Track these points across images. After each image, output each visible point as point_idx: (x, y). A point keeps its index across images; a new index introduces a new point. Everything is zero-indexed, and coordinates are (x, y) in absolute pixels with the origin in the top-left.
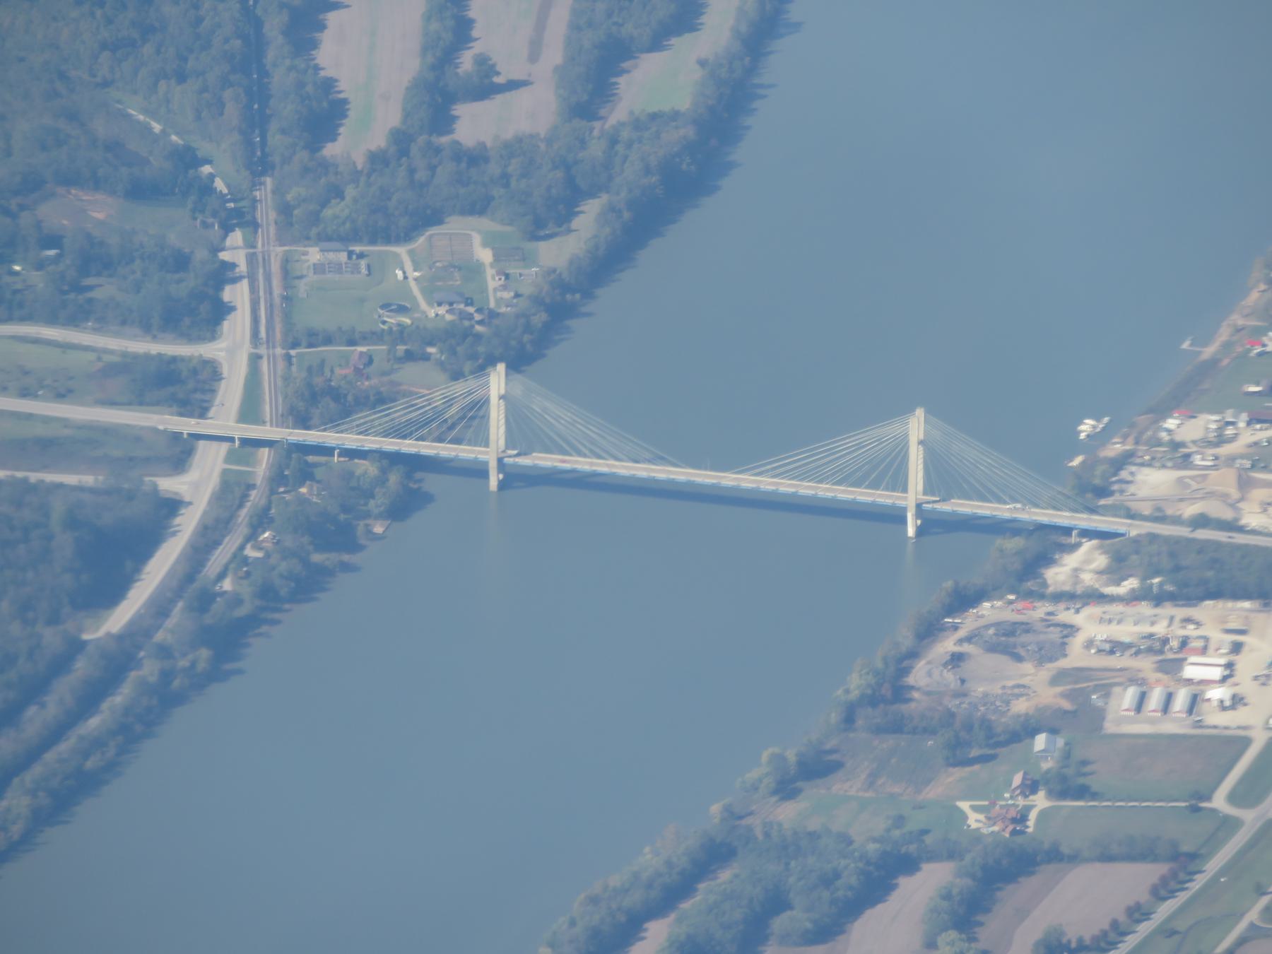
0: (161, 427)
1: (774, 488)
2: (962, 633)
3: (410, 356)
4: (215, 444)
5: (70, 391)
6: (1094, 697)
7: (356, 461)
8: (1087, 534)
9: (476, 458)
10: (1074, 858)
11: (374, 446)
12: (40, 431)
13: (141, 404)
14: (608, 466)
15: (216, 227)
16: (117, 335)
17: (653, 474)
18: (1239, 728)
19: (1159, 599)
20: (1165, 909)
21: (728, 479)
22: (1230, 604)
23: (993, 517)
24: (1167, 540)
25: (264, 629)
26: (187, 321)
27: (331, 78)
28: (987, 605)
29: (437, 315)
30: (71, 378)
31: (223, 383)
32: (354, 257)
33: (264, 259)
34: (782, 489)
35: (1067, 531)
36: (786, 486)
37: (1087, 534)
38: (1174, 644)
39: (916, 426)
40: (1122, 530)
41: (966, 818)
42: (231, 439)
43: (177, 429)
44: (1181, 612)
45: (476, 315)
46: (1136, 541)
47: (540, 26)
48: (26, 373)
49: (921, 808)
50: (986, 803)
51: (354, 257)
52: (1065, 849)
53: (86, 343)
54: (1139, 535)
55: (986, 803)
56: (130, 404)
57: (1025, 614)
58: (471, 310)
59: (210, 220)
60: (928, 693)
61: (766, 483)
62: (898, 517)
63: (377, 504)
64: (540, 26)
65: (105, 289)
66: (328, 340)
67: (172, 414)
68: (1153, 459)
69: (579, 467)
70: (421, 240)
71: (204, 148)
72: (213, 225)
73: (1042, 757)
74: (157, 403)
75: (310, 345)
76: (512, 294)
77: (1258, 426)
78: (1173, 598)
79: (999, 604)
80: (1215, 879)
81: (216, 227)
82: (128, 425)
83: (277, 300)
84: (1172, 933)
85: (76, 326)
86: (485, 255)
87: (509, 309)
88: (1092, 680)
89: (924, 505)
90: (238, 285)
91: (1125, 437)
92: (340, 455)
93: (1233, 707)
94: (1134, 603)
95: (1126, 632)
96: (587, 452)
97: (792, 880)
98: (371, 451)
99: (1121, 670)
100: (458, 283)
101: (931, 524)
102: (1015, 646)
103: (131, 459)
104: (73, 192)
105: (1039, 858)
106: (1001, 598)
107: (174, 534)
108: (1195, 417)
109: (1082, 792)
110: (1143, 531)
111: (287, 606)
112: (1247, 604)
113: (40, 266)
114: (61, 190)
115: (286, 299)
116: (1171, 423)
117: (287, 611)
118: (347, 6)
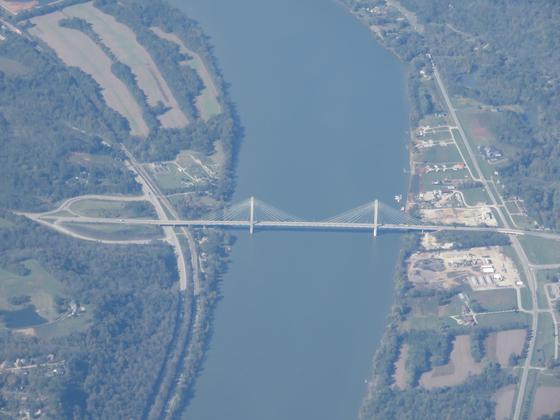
0: (152, 224)
1: (335, 226)
2: (413, 264)
3: (201, 195)
4: (168, 227)
5: (120, 215)
6: (464, 280)
7: (209, 228)
8: (426, 231)
9: (364, 227)
10: (497, 330)
11: (215, 224)
12: (121, 228)
13: (141, 217)
14: (285, 223)
15: (121, 160)
16: (115, 196)
17: (299, 225)
18: (509, 286)
19: (458, 248)
20: (532, 343)
21: (321, 224)
22: (478, 249)
23: (269, 225)
24: (450, 231)
25: (220, 283)
26: (134, 190)
27: (430, 114)
28: (413, 255)
29: (199, 181)
30: (118, 211)
31: (156, 208)
32: (164, 166)
33: (138, 168)
34: (337, 226)
35: (421, 231)
36: (338, 225)
37: (426, 231)
38: (474, 262)
39: (376, 205)
40: (436, 229)
41: (456, 321)
42: (173, 225)
43: (156, 224)
44: (467, 252)
45: (210, 180)
46: (442, 232)
47: (161, 90)
48: (105, 210)
49: (442, 319)
50: (459, 316)
51: (164, 166)
52: (493, 328)
53: (108, 199)
54: (441, 230)
55: (459, 316)
56: (138, 217)
57: (425, 257)
58: (208, 179)
59: (119, 158)
60: (417, 284)
61: (332, 225)
62: (371, 231)
63: (226, 241)
64: (161, 90)
65: (106, 182)
66: (175, 192)
67: (152, 219)
68: (424, 206)
69: (277, 225)
70: (177, 158)
71: (100, 136)
72: (120, 160)
73: (464, 300)
74: (144, 216)
75: (172, 194)
76: (215, 173)
77: (445, 194)
78: (462, 248)
79: (416, 254)
80: (538, 333)
81: (121, 160)
82: (143, 224)
83: (152, 181)
84: (539, 351)
85: (104, 194)
86: (198, 162)
87: (218, 177)
88: (459, 275)
89: (255, 224)
90: (138, 177)
91: (410, 200)
92: (205, 227)
93: (503, 280)
94: (452, 251)
95: (458, 259)
96: (278, 220)
97: (430, 346)
98: (215, 225)
99: (464, 271)
100: (198, 171)
101: (256, 229)
102: (430, 267)
103: (150, 234)
104: (75, 153)
105: (487, 332)
106: (416, 253)
107: (178, 256)
108: (426, 193)
109: (483, 311)
110: (443, 229)
111: (221, 275)
112: (483, 248)
113: (84, 177)
114: (72, 153)
115: (154, 180)
116: (421, 195)
117: (222, 276)
118: (104, 89)
